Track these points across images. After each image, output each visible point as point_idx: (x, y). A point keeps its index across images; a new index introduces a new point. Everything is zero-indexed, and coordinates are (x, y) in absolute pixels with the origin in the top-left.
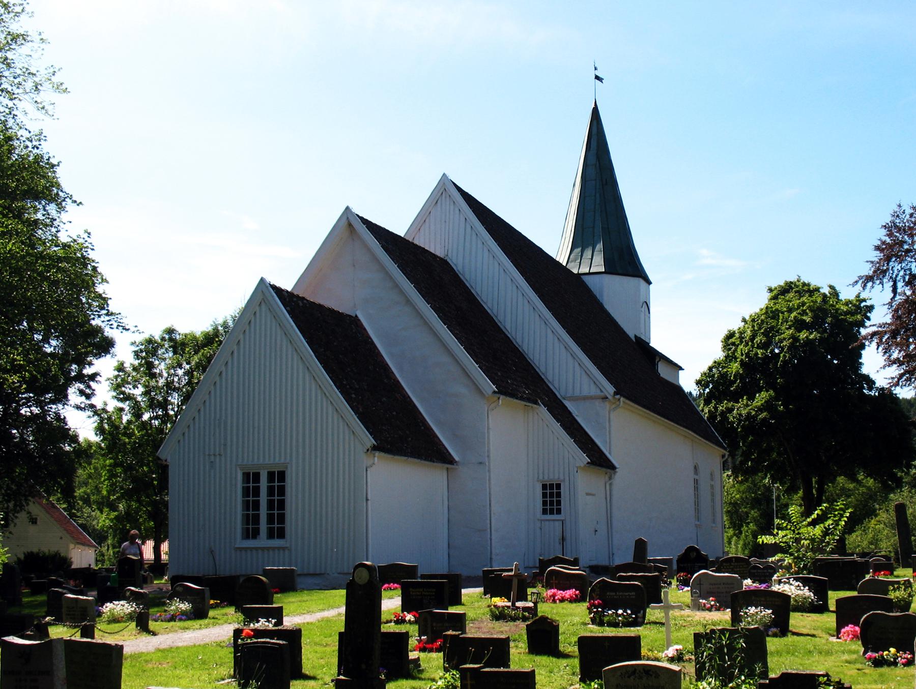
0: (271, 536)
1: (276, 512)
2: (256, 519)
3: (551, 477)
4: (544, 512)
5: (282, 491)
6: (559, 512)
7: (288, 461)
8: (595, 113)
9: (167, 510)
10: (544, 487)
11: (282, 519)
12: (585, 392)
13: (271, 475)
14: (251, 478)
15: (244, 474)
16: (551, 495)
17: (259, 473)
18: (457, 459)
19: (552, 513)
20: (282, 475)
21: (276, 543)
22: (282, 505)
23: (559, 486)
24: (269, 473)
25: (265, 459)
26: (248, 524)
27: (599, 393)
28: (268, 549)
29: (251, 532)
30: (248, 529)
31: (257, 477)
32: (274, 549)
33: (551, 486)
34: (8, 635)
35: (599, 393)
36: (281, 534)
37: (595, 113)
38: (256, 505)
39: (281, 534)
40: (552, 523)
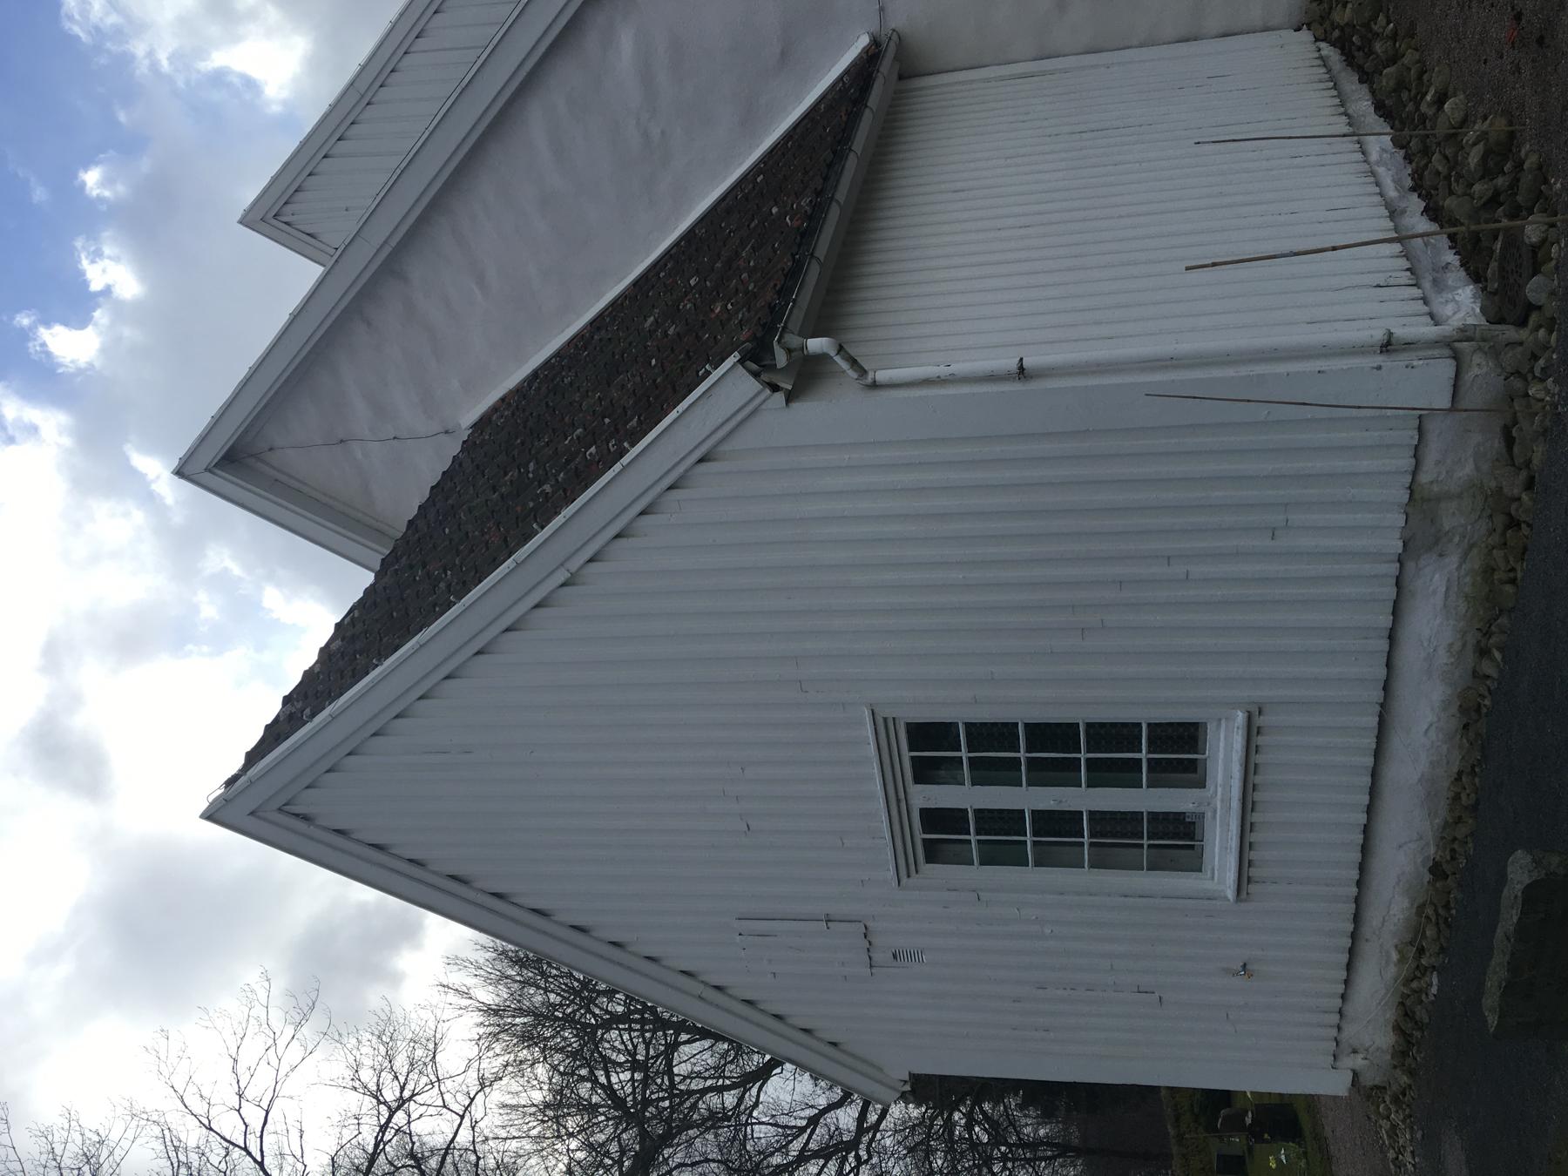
0: (1190, 772)
13: (925, 772)
14: (941, 835)
17: (925, 813)
18: (864, 41)
21: (1224, 752)
22: (1046, 735)
24: (919, 779)
25: (861, 795)
28: (1248, 788)
29: (1177, 839)
31: (935, 819)
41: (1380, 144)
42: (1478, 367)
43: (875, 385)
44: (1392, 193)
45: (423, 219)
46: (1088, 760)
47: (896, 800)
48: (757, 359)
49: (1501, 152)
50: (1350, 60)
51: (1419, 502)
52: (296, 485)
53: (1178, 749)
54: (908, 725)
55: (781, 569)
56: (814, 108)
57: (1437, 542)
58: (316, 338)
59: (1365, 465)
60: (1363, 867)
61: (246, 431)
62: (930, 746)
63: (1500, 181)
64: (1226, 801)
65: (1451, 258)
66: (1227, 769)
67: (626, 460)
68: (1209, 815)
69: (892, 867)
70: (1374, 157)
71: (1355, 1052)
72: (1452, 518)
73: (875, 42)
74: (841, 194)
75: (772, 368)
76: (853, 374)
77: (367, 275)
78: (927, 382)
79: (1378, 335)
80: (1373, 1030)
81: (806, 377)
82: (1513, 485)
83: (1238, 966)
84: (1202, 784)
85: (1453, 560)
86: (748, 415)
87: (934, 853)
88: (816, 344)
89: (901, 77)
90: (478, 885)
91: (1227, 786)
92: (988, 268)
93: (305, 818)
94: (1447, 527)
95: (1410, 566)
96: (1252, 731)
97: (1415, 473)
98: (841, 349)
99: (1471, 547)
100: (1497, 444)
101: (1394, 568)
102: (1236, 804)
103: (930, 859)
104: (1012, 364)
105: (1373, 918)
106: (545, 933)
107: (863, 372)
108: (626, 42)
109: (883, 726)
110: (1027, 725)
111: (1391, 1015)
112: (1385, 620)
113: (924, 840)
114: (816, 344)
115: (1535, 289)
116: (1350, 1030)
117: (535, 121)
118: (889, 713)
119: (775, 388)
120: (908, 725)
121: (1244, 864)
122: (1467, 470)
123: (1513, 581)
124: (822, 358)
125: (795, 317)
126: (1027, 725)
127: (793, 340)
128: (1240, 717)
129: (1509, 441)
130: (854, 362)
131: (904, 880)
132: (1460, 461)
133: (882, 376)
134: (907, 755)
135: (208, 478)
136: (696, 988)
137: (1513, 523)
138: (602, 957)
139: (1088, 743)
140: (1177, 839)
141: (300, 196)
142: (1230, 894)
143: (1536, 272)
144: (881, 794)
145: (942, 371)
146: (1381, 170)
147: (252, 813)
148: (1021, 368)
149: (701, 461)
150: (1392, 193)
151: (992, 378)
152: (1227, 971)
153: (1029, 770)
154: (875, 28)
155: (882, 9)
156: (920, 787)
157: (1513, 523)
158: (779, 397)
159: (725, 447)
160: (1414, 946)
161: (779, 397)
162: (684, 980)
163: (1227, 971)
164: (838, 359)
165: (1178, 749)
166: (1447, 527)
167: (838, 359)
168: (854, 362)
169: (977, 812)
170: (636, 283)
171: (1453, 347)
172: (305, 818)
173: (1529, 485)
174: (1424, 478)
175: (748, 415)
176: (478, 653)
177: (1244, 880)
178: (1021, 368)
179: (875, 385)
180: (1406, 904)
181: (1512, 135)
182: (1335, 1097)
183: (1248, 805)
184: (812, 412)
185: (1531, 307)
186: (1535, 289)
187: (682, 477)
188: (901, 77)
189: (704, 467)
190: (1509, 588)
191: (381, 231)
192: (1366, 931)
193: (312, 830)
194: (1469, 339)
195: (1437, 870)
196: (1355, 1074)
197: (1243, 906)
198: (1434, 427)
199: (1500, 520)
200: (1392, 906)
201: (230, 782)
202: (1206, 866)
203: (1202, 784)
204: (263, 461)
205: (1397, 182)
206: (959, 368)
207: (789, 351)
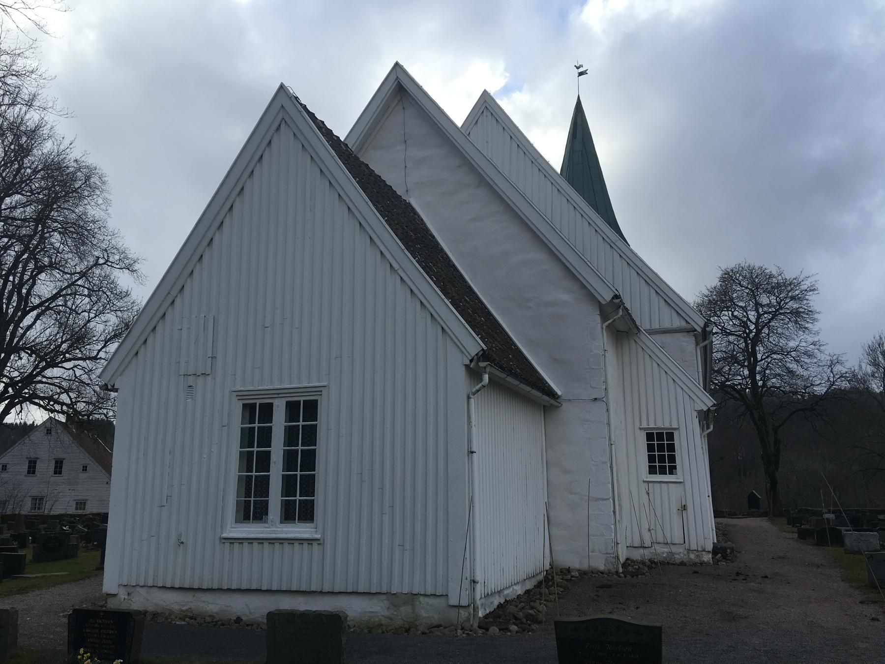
0: (288, 516)
1: (252, 499)
2: (263, 485)
3: (659, 425)
4: (652, 470)
5: (311, 435)
6: (672, 470)
7: (675, 426)
8: (579, 108)
9: (112, 450)
10: (650, 437)
11: (309, 485)
12: (667, 325)
13: (292, 408)
14: (257, 412)
16: (661, 448)
17: (270, 406)
18: (559, 393)
19: (663, 471)
20: (311, 409)
21: (299, 530)
22: (310, 461)
23: (671, 436)
24: (289, 404)
26: (248, 495)
27: (684, 324)
28: (281, 541)
29: (252, 509)
31: (267, 411)
33: (660, 436)
34: (5, 336)
35: (684, 324)
36: (307, 514)
37: (579, 108)
38: (264, 461)
39: (307, 514)
41: (519, 590)
42: (464, 614)
43: (469, 398)
44: (506, 592)
47: (278, 393)
48: (483, 356)
49: (534, 620)
51: (413, 597)
57: (395, 606)
58: (480, 170)
59: (429, 576)
61: (413, 99)
63: (524, 620)
65: (488, 612)
66: (292, 532)
68: (267, 525)
70: (515, 587)
71: (129, 594)
73: (559, 397)
75: (478, 360)
76: (474, 390)
77: (482, 172)
78: (469, 417)
81: (474, 373)
86: (461, 349)
87: (249, 408)
88: (486, 377)
90: (237, 199)
91: (282, 532)
93: (278, 128)
95: (384, 597)
96: (310, 541)
97: (426, 595)
98: (484, 386)
99: (391, 619)
101: (384, 590)
103: (244, 406)
104: (474, 449)
105: (208, 597)
107: (474, 394)
108: (566, 297)
109: (318, 390)
110: (315, 450)
111: (151, 608)
112: (361, 589)
114: (486, 377)
115: (494, 630)
116: (142, 591)
117: (538, 255)
119: (471, 361)
120: (317, 401)
121: (241, 541)
122: (424, 614)
124: (481, 380)
126: (315, 450)
127: (488, 370)
128: (318, 536)
129: (439, 626)
131: (235, 394)
132: (428, 612)
133: (472, 401)
136: (174, 293)
137: (407, 631)
139: (260, 476)
142: (225, 535)
145: (473, 424)
148: (472, 452)
150: (506, 592)
151: (470, 441)
152: (180, 535)
153: (248, 451)
157: (407, 631)
158: (468, 362)
160: (191, 617)
161: (468, 362)
162: (179, 286)
163: (180, 535)
164: (480, 385)
167: (480, 385)
168: (478, 391)
169: (271, 428)
172: (278, 128)
173: (423, 633)
174: (422, 599)
175: (461, 349)
177: (232, 541)
178: (472, 452)
179: (469, 398)
180: (215, 611)
181: (540, 622)
182: (101, 585)
183: (272, 541)
184: (460, 374)
185: (487, 629)
186: (494, 630)
189: (440, 330)
190: (380, 631)
192: (198, 595)
195: (239, 620)
196: (114, 595)
197: (217, 542)
198: (442, 601)
199: (407, 626)
200: (212, 605)
201: (296, 98)
204: (399, 101)
205: (507, 595)
206: (474, 430)
207: (485, 368)
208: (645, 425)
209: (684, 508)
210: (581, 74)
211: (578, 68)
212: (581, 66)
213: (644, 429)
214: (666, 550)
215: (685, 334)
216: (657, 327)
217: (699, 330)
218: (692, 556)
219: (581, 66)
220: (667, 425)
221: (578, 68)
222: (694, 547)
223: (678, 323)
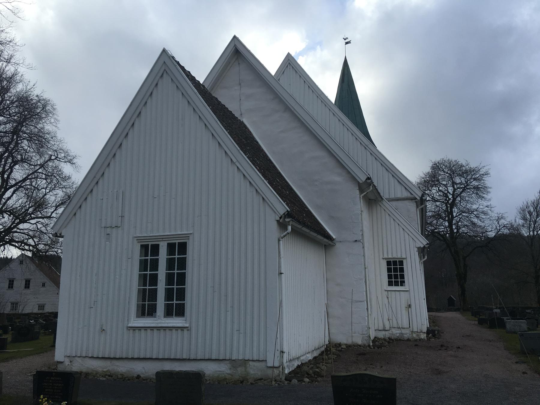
0: (169, 313)
2: (153, 294)
3: (395, 256)
4: (390, 284)
5: (182, 264)
6: (402, 283)
7: (404, 256)
8: (346, 65)
10: (389, 263)
11: (181, 294)
12: (399, 195)
13: (171, 247)
14: (149, 250)
15: (142, 246)
17: (158, 246)
18: (334, 237)
19: (396, 284)
20: (183, 247)
21: (176, 322)
22: (182, 279)
23: (401, 263)
24: (169, 245)
25: (163, 228)
26: (144, 300)
27: (409, 195)
28: (165, 328)
29: (147, 309)
30: (144, 306)
31: (155, 249)
32: (171, 328)
33: (395, 263)
35: (409, 195)
36: (180, 312)
37: (346, 65)
38: (154, 280)
40: (398, 293)
41: (310, 357)
42: (276, 372)
43: (279, 240)
44: (302, 358)
45: (299, 120)
46: (174, 288)
47: (163, 238)
48: (288, 215)
49: (319, 375)
50: (323, 352)
51: (245, 362)
52: (229, 68)
53: (176, 309)
54: (186, 243)
55: (220, 212)
56: (320, 224)
60: (133, 359)
61: (245, 58)
62: (178, 248)
63: (313, 375)
64: (160, 323)
67: (265, 181)
68: (155, 319)
69: (140, 235)
71: (71, 362)
72: (240, 371)
74: (312, 233)
75: (285, 218)
76: (282, 236)
78: (279, 252)
79: (285, 350)
80: (77, 366)
81: (282, 225)
82: (250, 381)
83: (104, 328)
84: (164, 317)
85: (229, 372)
87: (144, 248)
88: (290, 228)
89: (325, 245)
91: (165, 323)
92: (297, 267)
93: (162, 76)
94: (238, 369)
96: (182, 328)
97: (253, 361)
98: (288, 233)
99: (232, 375)
100: (259, 378)
101: (228, 358)
102: (160, 325)
103: (142, 246)
104: (282, 272)
106: (120, 136)
107: (282, 238)
108: (338, 179)
109: (187, 236)
111: (84, 370)
113: (148, 245)
114: (290, 228)
115: (294, 381)
117: (321, 153)
118: (190, 238)
119: (280, 218)
120: (186, 243)
121: (140, 328)
122: (252, 372)
123: (227, 383)
124: (287, 229)
125: (294, 224)
127: (291, 223)
128: (187, 325)
129: (261, 379)
130: (285, 236)
131: (136, 239)
132: (254, 370)
133: (281, 242)
134: (177, 242)
135: (233, 45)
136: (98, 176)
138: (111, 150)
140: (147, 309)
141: (295, 72)
142: (130, 325)
143: (298, 381)
144: (165, 234)
145: (282, 256)
146: (305, 356)
147: (164, 62)
148: (281, 274)
149: (263, 198)
150: (302, 358)
151: (280, 267)
152: (102, 325)
154: (337, 240)
155: (340, 242)
156: (166, 244)
157: (242, 382)
158: (278, 219)
159: (266, 204)
161: (278, 219)
163: (102, 325)
164: (286, 232)
165: (176, 309)
166: (238, 369)
167: (286, 232)
168: (285, 236)
169: (158, 259)
170: (280, 173)
171: (281, 366)
172: (162, 76)
174: (251, 363)
175: (275, 212)
176: (213, 134)
177: (134, 328)
178: (281, 274)
179: (279, 240)
180: (124, 371)
181: (323, 376)
183: (159, 328)
184: (274, 226)
186: (294, 381)
187: (259, 193)
188: (325, 245)
191: (297, 108)
193: (158, 78)
194: (282, 369)
195: (138, 377)
196: (62, 362)
197: (125, 329)
199: (242, 379)
200: (122, 368)
201: (173, 57)
202: (138, 319)
203: (164, 317)
206: (282, 260)
208: (386, 256)
209: (410, 306)
210: (347, 43)
211: (345, 39)
212: (347, 38)
213: (386, 259)
214: (398, 332)
215: (410, 201)
216: (393, 197)
217: (419, 198)
218: (414, 335)
219: (347, 38)
220: (399, 256)
221: (345, 39)
222: (415, 330)
223: (406, 194)
